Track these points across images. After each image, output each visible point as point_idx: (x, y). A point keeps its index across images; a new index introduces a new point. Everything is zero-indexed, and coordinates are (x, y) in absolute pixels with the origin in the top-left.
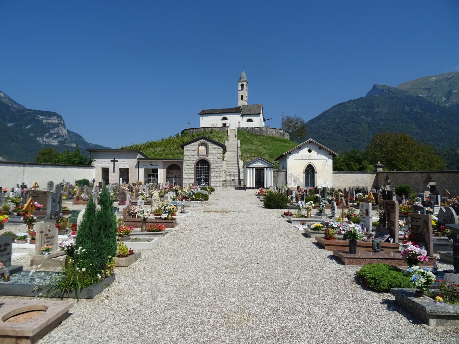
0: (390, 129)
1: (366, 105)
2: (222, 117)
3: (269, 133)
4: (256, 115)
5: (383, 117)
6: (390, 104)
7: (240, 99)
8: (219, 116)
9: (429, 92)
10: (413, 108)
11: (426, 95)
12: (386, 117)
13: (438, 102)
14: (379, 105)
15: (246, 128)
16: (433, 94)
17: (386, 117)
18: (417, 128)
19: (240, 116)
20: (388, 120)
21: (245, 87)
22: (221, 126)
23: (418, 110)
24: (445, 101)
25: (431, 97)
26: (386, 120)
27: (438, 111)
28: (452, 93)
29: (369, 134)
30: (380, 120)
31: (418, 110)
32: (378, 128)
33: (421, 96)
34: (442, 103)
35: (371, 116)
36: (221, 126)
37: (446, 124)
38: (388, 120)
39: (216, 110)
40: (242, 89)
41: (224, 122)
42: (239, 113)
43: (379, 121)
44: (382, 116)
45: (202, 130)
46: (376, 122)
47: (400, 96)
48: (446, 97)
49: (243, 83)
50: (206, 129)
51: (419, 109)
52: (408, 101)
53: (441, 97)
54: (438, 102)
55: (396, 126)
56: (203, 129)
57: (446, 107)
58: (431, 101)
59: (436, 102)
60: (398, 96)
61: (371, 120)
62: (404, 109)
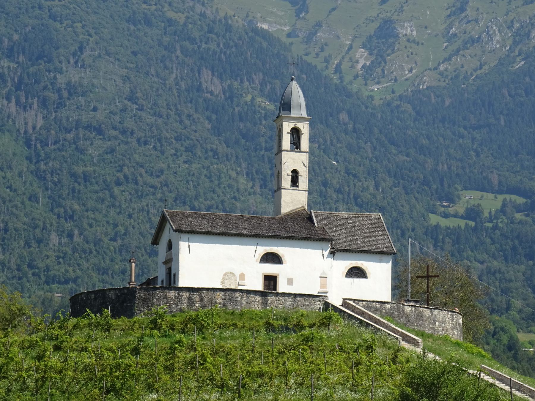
0: (136, 182)
1: (16, 37)
2: (262, 250)
3: (440, 326)
4: (378, 256)
5: (101, 115)
6: (134, 53)
7: (286, 182)
8: (253, 248)
9: (298, 15)
10: (236, 85)
11: (287, 29)
12: (117, 118)
13: (338, 70)
14: (81, 49)
15: (378, 305)
16: (319, 25)
17: (117, 118)
18: (257, 189)
19: (326, 253)
20: (124, 132)
21: (305, 143)
22: (259, 286)
23: (259, 100)
24: (368, 70)
25: (308, 40)
26: (113, 133)
27: (343, 116)
28: (397, 36)
29: (33, 198)
30: (88, 127)
31: (259, 100)
32: (79, 169)
33: (265, 26)
34: (356, 77)
35: (44, 103)
36: (259, 286)
37: (377, 186)
38: (124, 132)
39: (366, 254)
40: (296, 144)
41: (271, 269)
42: (324, 244)
43: (81, 132)
44: (95, 109)
45: (219, 297)
46: (70, 136)
47: (181, 18)
48: (371, 54)
49: (299, 125)
50: (237, 294)
51: (262, 93)
52: (213, 46)
53: (351, 48)
54: (338, 70)
55: (162, 172)
56: (221, 294)
57: (372, 97)
58: (309, 59)
59: (332, 68)
60: (171, 14)
61: (40, 123)
62: (199, 89)
